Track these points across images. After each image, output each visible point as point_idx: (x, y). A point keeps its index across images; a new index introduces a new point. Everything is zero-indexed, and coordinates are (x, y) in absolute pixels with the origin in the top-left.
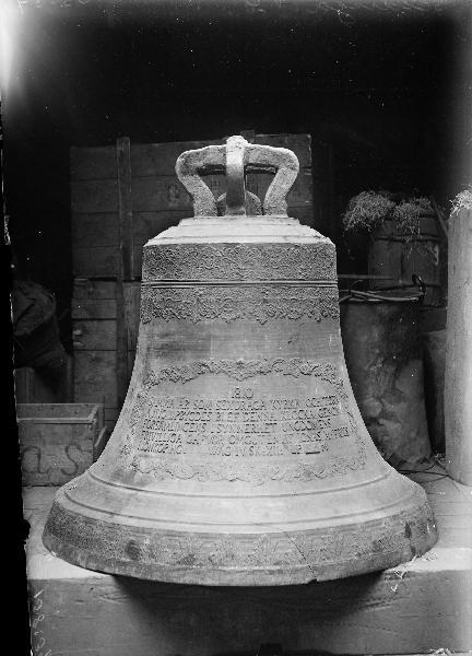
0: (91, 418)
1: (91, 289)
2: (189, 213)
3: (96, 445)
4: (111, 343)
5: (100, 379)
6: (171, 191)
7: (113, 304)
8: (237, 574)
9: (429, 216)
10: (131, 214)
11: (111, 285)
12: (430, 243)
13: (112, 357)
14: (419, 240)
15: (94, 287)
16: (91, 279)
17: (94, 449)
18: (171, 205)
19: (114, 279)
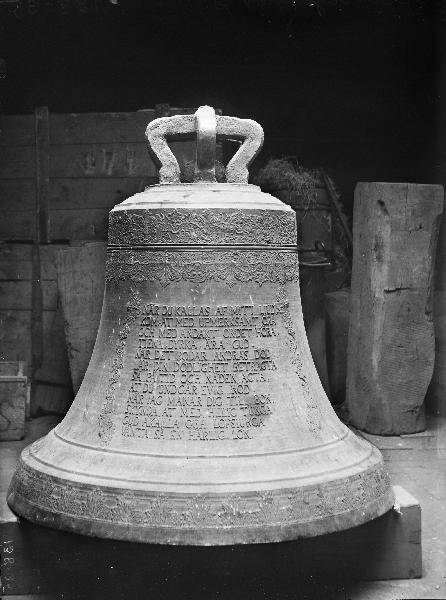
0: (20, 375)
1: (7, 251)
2: (154, 180)
3: (28, 402)
4: (26, 302)
5: (15, 337)
6: (88, 159)
7: (29, 265)
8: (217, 533)
9: (321, 187)
10: (48, 180)
11: (28, 248)
12: (324, 212)
13: (26, 316)
14: (317, 209)
15: (11, 249)
16: (7, 242)
17: (26, 405)
18: (87, 172)
19: (31, 242)
